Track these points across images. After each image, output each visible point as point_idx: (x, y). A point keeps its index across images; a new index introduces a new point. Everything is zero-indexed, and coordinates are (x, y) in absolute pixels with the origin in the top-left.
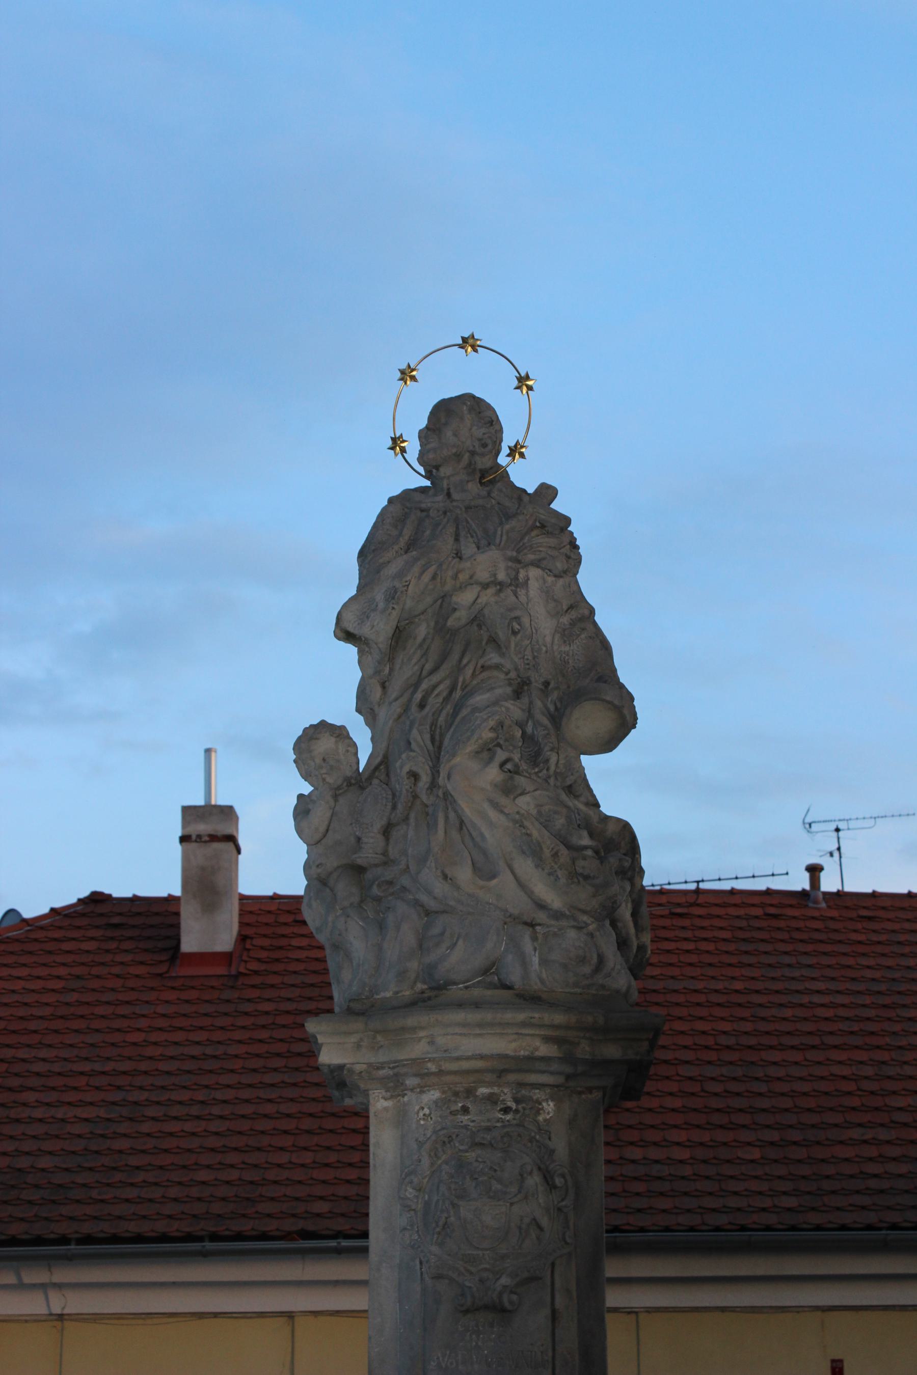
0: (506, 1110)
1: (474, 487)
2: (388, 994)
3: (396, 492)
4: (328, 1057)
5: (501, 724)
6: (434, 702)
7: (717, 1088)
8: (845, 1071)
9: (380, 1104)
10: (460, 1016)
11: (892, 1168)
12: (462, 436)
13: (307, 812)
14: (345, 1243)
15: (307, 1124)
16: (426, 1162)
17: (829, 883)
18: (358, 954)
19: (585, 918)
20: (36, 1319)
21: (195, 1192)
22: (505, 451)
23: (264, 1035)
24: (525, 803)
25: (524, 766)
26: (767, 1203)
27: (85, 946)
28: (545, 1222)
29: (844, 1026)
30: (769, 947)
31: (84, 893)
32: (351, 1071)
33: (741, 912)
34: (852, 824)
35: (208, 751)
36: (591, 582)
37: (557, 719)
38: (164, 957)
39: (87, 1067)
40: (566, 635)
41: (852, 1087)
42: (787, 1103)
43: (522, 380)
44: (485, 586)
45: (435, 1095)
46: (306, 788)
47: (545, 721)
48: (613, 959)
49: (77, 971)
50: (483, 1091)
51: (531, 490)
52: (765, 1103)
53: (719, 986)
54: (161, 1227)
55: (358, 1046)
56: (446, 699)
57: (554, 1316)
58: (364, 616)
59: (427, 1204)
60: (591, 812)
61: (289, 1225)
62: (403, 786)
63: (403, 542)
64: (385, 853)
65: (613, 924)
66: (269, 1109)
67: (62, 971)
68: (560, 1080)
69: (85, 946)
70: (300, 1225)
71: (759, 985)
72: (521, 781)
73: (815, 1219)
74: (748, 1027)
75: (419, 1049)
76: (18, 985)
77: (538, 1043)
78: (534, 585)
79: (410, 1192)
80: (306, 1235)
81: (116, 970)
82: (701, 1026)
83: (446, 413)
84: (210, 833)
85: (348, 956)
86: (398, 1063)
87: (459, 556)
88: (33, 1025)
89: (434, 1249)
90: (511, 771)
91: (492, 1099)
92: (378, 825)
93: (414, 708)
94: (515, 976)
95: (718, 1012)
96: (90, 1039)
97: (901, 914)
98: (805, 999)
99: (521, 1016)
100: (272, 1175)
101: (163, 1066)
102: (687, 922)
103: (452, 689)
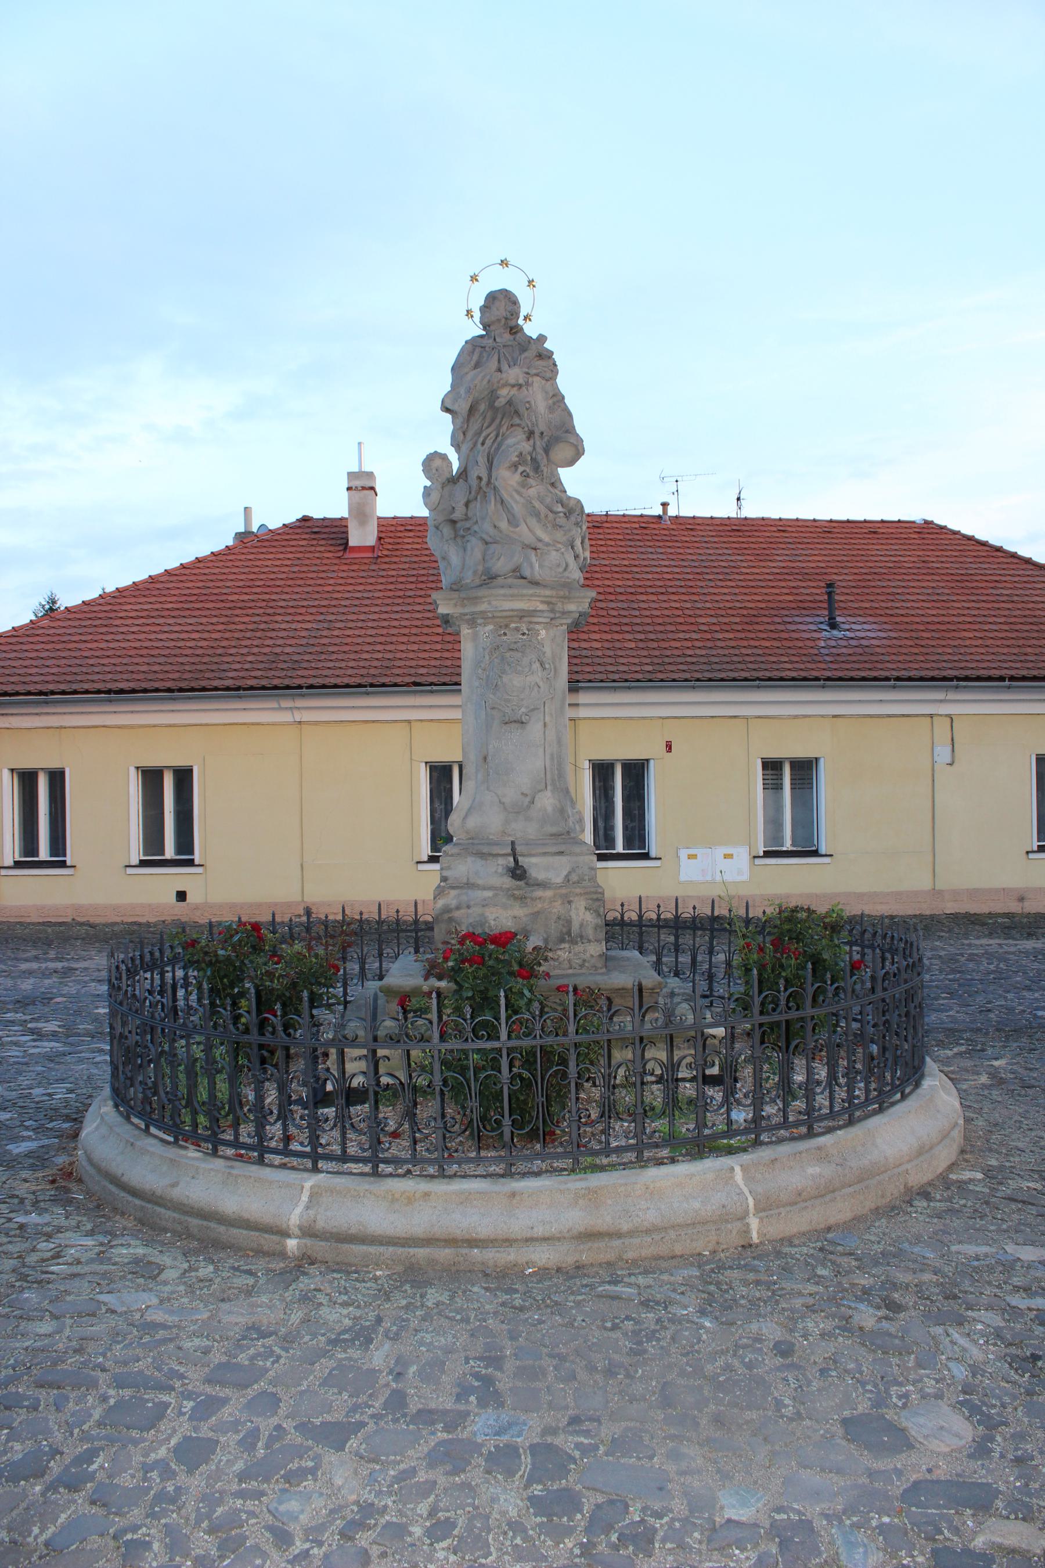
0: (524, 634)
1: (507, 336)
2: (468, 581)
3: (469, 338)
4: (442, 610)
5: (521, 454)
6: (488, 442)
7: (615, 613)
8: (677, 605)
9: (465, 631)
10: (502, 591)
11: (698, 652)
12: (501, 312)
13: (429, 495)
14: (435, 688)
15: (414, 631)
16: (487, 657)
17: (672, 512)
18: (454, 560)
19: (560, 546)
20: (289, 724)
21: (362, 664)
22: (521, 317)
23: (392, 587)
24: (532, 492)
25: (531, 474)
26: (638, 668)
27: (301, 543)
28: (541, 684)
29: (678, 583)
30: (642, 544)
31: (299, 516)
32: (452, 617)
33: (628, 526)
34: (685, 478)
35: (360, 444)
36: (563, 382)
37: (547, 451)
38: (341, 548)
39: (305, 603)
40: (551, 409)
41: (680, 613)
42: (649, 621)
43: (531, 283)
44: (513, 386)
45: (491, 627)
46: (428, 483)
47: (542, 452)
48: (573, 565)
49: (297, 556)
50: (513, 625)
51: (534, 337)
52: (638, 621)
53: (617, 563)
54: (346, 681)
55: (456, 605)
56: (494, 441)
57: (545, 725)
58: (455, 400)
59: (488, 676)
60: (563, 495)
61: (408, 679)
62: (474, 483)
63: (473, 363)
64: (466, 515)
65: (572, 548)
66: (396, 623)
67: (290, 556)
68: (548, 620)
69: (301, 543)
70: (413, 679)
71: (637, 563)
72: (531, 481)
73: (661, 676)
74: (630, 583)
75: (483, 607)
76: (269, 563)
77: (538, 604)
78: (536, 385)
79: (480, 671)
80: (416, 684)
81: (317, 555)
82: (607, 582)
83: (493, 298)
84: (362, 486)
85: (449, 564)
86: (474, 613)
87: (499, 370)
88: (278, 583)
89: (491, 696)
90: (525, 475)
91: (517, 629)
92: (463, 501)
93: (479, 445)
94: (527, 573)
95: (616, 576)
96: (306, 589)
97: (708, 528)
98: (658, 570)
99: (531, 592)
100: (398, 655)
101: (343, 603)
102: (600, 531)
103: (497, 436)
